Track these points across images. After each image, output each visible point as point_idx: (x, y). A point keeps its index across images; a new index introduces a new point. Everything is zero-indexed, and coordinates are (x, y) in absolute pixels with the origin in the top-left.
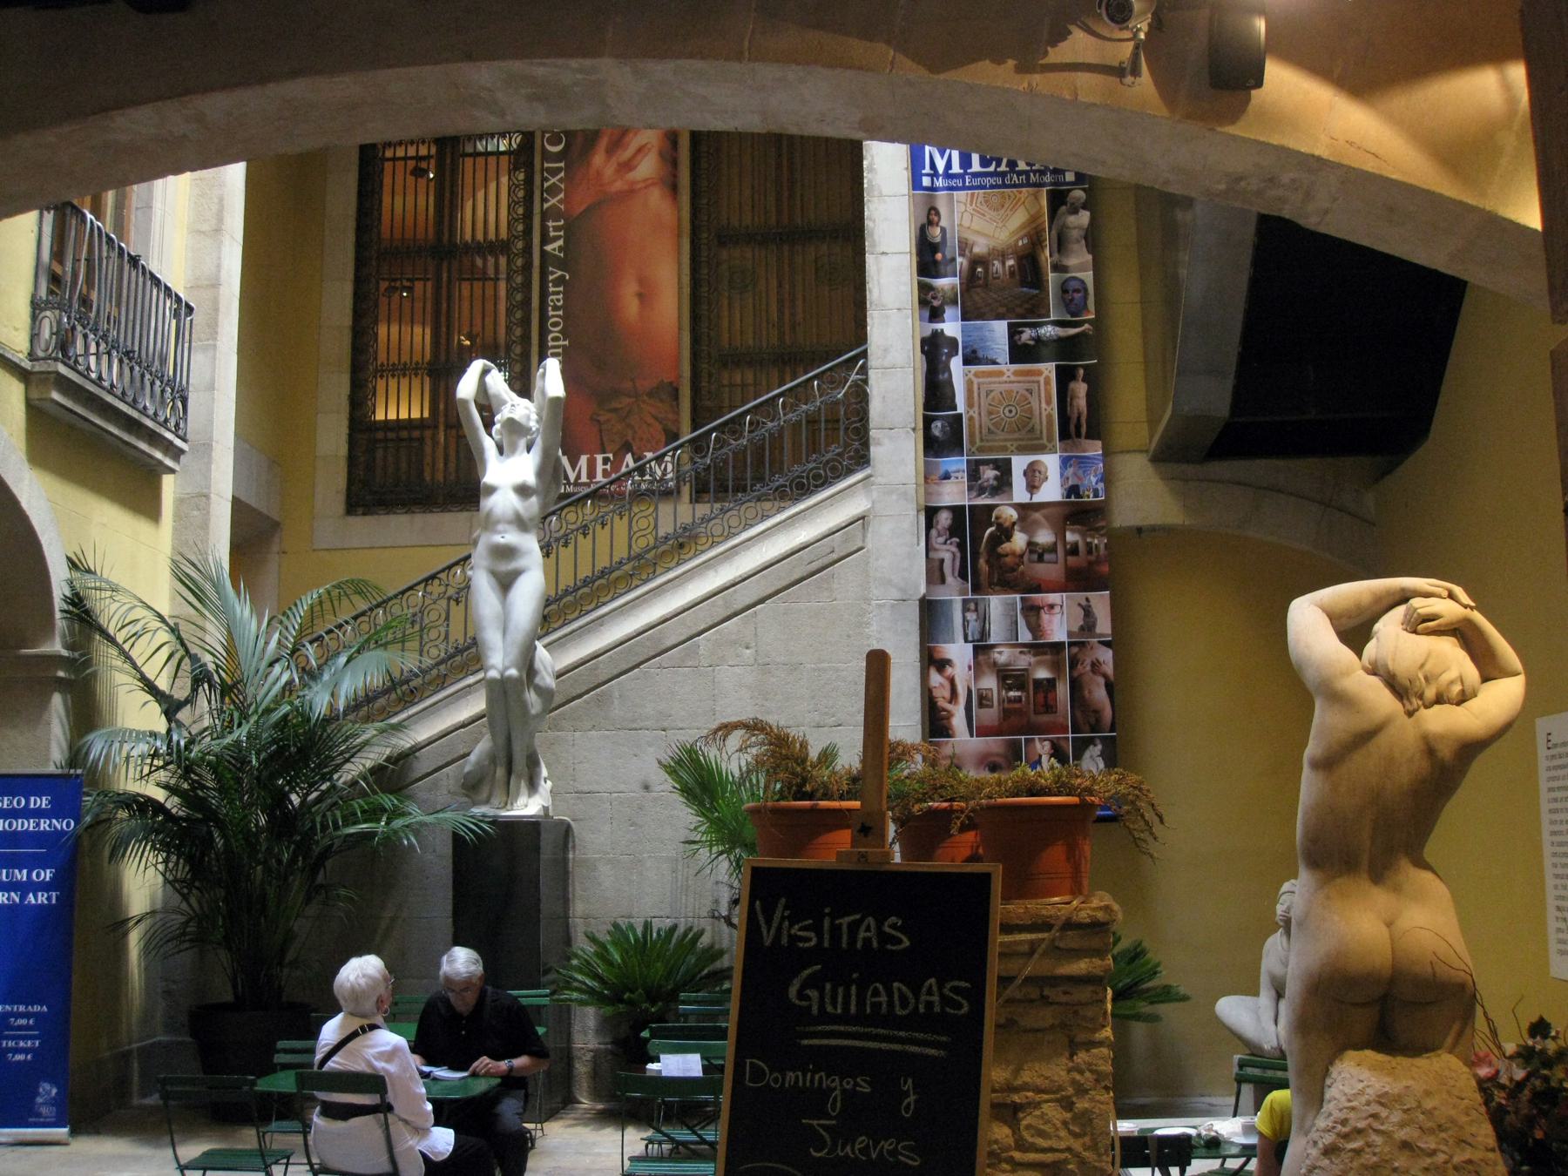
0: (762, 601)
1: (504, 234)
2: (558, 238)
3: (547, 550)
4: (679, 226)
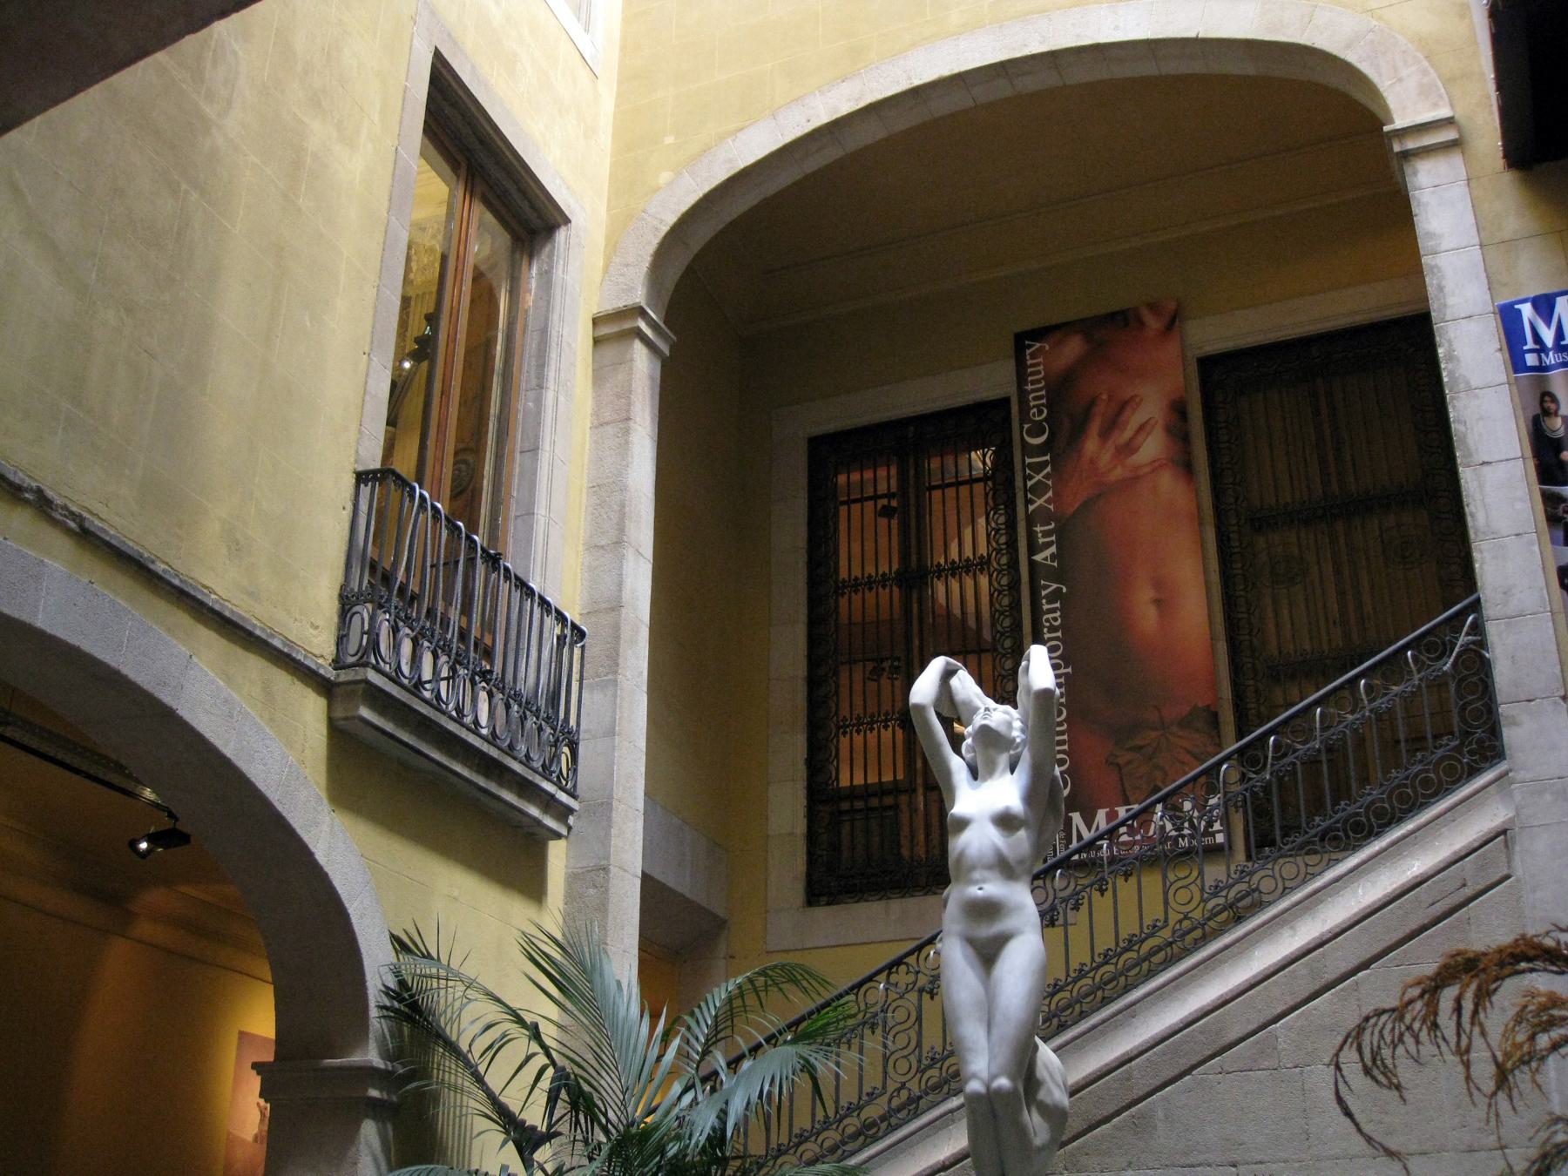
0: (1365, 965)
1: (983, 550)
2: (1048, 545)
3: (1049, 918)
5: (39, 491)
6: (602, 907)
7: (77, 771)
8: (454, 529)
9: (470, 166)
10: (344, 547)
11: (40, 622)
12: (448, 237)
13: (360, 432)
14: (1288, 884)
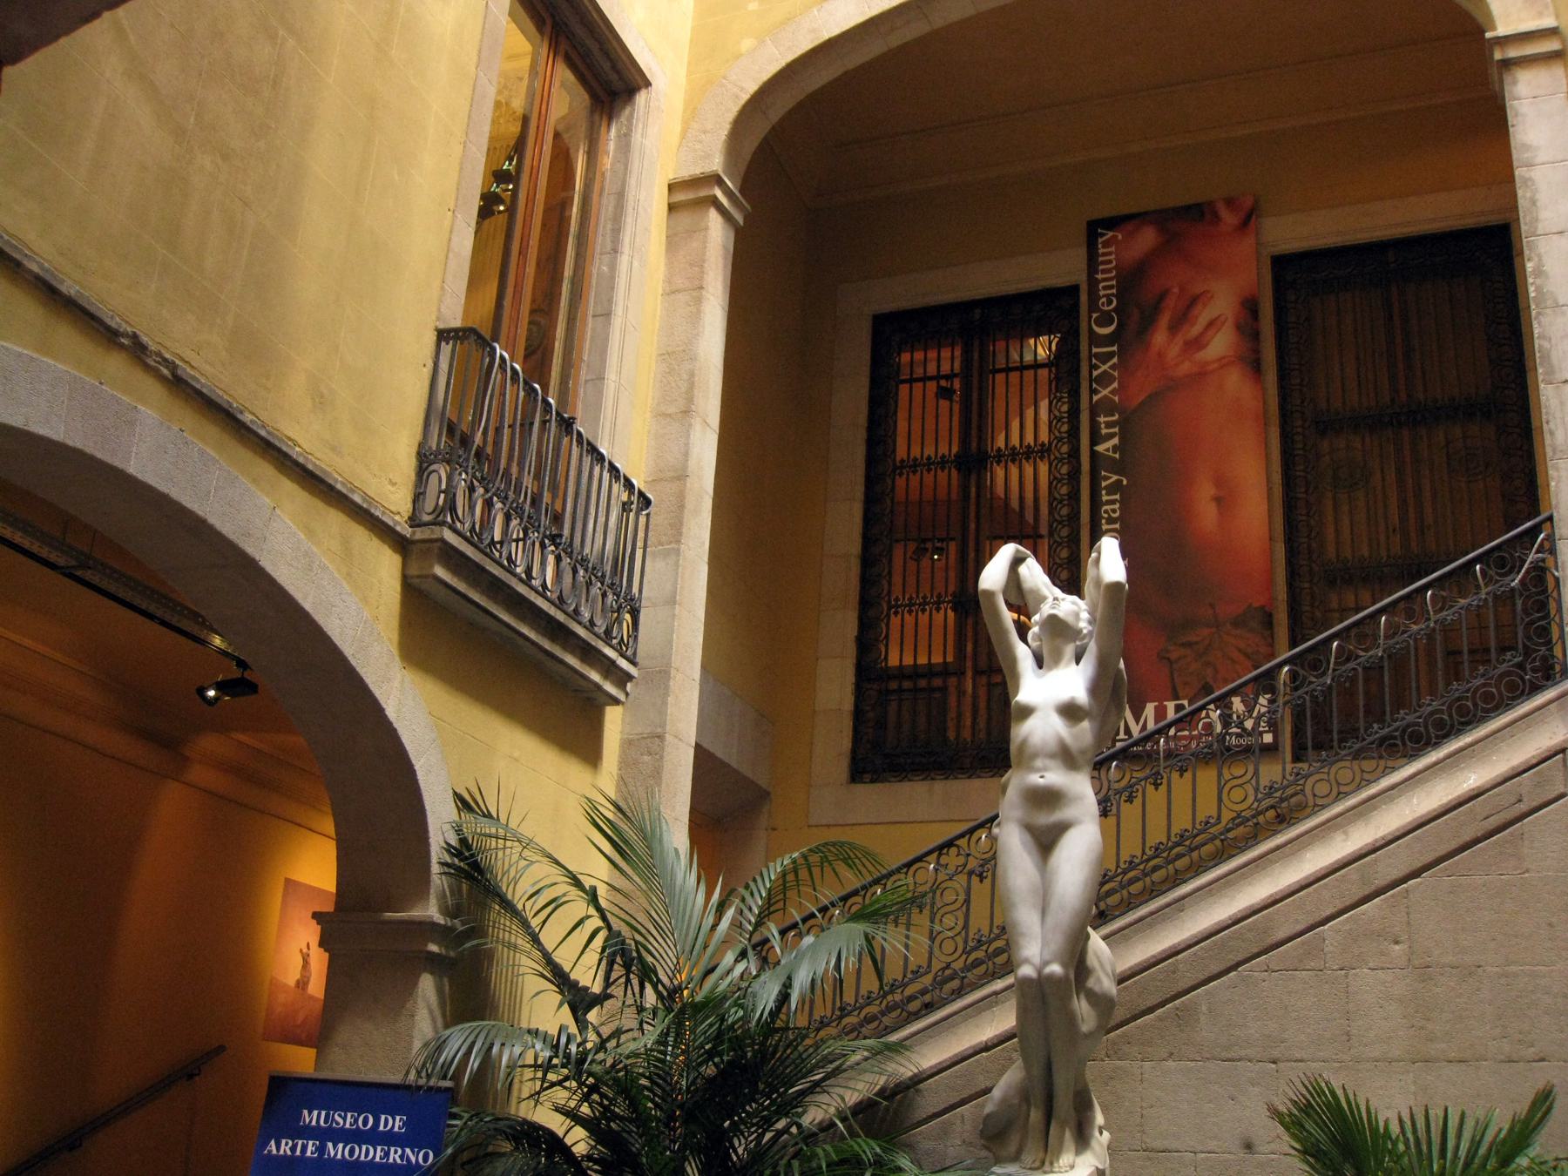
0: (1416, 874)
1: (1044, 436)
2: (1111, 436)
4: (1265, 412)
5: (135, 336)
6: (657, 773)
7: (151, 617)
8: (531, 391)
9: (555, 25)
10: (424, 406)
11: (133, 468)
12: (531, 94)
13: (442, 288)
14: (1342, 789)
